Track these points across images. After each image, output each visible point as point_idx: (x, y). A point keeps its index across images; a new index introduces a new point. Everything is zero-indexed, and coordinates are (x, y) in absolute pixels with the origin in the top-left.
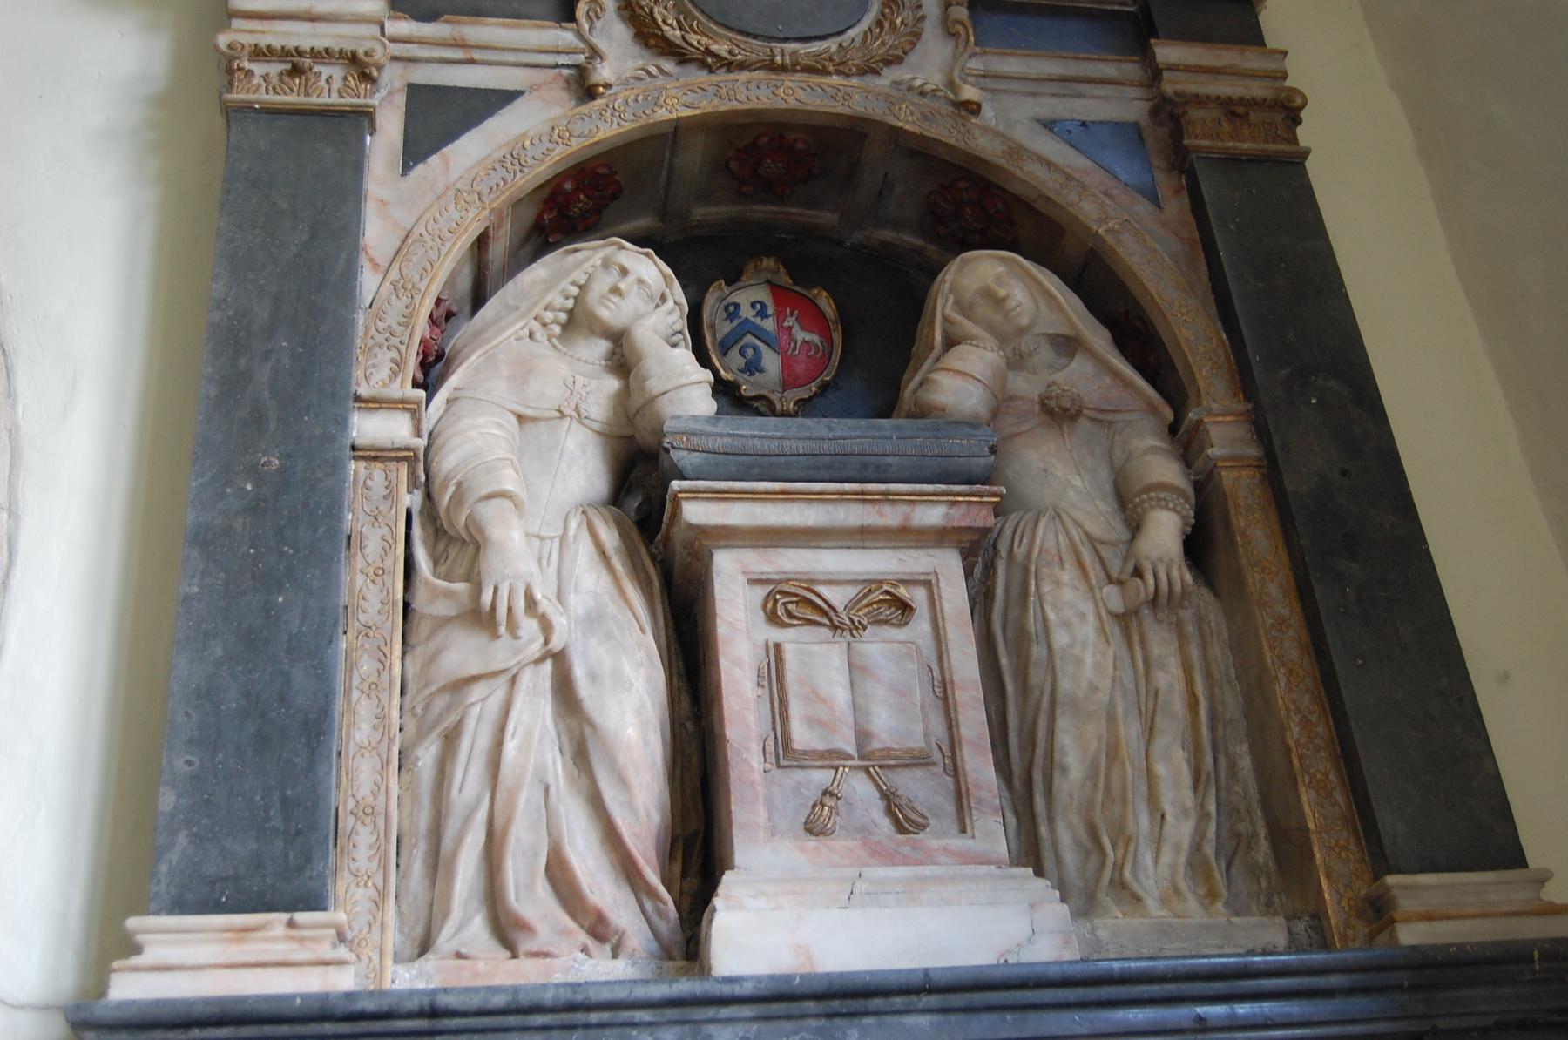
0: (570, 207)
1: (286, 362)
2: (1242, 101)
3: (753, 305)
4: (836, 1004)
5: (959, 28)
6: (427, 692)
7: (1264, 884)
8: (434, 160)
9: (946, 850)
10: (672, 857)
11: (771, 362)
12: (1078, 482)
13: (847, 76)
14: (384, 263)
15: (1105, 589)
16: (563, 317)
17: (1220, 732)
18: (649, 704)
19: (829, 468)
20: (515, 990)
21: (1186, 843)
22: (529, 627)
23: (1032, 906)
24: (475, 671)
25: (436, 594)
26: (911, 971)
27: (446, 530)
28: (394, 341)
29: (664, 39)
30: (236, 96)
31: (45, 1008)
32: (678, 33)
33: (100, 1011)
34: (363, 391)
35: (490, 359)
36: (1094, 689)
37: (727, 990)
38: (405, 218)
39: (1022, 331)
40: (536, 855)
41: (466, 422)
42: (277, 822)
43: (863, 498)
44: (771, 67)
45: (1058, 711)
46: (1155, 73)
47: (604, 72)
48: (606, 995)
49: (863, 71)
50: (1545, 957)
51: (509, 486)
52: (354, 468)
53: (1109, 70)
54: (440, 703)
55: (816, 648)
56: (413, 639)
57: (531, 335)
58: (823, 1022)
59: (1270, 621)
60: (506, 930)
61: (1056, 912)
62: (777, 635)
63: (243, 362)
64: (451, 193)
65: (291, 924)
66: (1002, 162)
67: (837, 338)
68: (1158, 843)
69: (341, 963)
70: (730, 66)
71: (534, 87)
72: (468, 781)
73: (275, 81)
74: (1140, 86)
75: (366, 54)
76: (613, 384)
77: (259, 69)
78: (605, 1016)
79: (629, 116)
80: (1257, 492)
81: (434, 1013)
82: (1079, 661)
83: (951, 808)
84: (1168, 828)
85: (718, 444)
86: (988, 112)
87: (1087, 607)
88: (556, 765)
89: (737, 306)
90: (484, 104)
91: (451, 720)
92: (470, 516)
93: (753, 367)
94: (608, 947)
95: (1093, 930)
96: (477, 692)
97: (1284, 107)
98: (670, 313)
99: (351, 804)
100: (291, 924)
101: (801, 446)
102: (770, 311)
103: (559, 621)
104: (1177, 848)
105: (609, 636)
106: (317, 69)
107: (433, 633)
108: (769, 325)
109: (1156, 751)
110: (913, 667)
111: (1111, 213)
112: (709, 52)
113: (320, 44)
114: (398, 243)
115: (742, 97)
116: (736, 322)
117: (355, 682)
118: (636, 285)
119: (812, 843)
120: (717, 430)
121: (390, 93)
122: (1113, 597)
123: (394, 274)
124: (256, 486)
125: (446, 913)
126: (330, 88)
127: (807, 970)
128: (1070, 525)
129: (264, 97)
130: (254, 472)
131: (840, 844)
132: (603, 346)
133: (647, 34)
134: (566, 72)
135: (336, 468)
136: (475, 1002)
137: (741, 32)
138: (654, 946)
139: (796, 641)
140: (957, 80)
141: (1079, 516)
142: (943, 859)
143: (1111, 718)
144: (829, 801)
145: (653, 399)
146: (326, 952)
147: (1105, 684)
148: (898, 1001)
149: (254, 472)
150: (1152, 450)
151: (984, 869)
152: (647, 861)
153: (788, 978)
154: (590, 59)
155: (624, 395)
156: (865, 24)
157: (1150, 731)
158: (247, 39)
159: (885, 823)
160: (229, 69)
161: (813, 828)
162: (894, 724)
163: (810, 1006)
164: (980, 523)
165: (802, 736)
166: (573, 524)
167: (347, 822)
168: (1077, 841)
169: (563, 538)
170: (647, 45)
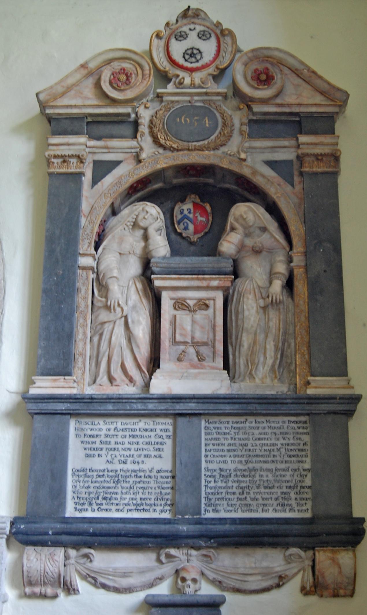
0: (140, 190)
1: (63, 245)
2: (321, 155)
3: (188, 210)
4: (174, 400)
6: (96, 325)
8: (99, 184)
9: (209, 366)
11: (191, 227)
12: (259, 270)
13: (210, 151)
14: (87, 215)
15: (260, 301)
16: (132, 224)
18: (146, 328)
19: (191, 271)
20: (108, 395)
22: (118, 310)
23: (222, 381)
24: (106, 320)
25: (98, 301)
26: (190, 395)
27: (101, 284)
29: (159, 143)
30: (51, 170)
32: (164, 141)
34: (81, 252)
35: (113, 236)
36: (252, 326)
38: (92, 201)
39: (250, 227)
40: (118, 363)
41: (106, 256)
42: (62, 357)
43: (198, 279)
44: (189, 150)
45: (243, 332)
47: (143, 156)
48: (126, 396)
49: (214, 149)
50: (340, 398)
52: (79, 271)
53: (286, 143)
54: (99, 327)
55: (184, 316)
56: (93, 310)
57: (124, 229)
58: (172, 404)
59: (298, 311)
60: (111, 379)
62: (175, 312)
63: (53, 246)
64: (103, 194)
67: (210, 218)
68: (264, 364)
69: (74, 387)
71: (126, 159)
73: (60, 164)
74: (295, 147)
75: (82, 156)
77: (55, 161)
78: (126, 401)
79: (150, 168)
81: (92, 398)
82: (250, 319)
83: (212, 355)
84: (267, 361)
85: (164, 265)
86: (249, 160)
87: (254, 305)
88: (124, 342)
89: (183, 210)
91: (101, 332)
92: (106, 282)
93: (186, 228)
94: (133, 384)
95: (240, 386)
96: (106, 325)
97: (333, 155)
98: (159, 223)
99: (78, 352)
100: (64, 379)
102: (192, 211)
103: (125, 308)
104: (268, 366)
105: (137, 312)
108: (191, 216)
110: (206, 321)
111: (279, 191)
112: (171, 147)
113: (70, 153)
114: (90, 209)
115: (180, 160)
116: (183, 215)
117: (79, 324)
118: (152, 213)
119: (178, 363)
120: (164, 262)
121: (89, 163)
122: (262, 303)
123: (89, 218)
124: (57, 278)
125: (99, 375)
126: (73, 167)
127: (170, 393)
128: (254, 283)
130: (56, 275)
131: (184, 364)
132: (142, 232)
133: (156, 141)
134: (134, 154)
135: (75, 273)
136: (100, 397)
137: (181, 140)
138: (144, 384)
139: (180, 314)
140: (240, 151)
142: (208, 368)
143: (255, 334)
144: (183, 353)
145: (150, 251)
146: (72, 385)
147: (255, 325)
148: (188, 400)
149: (56, 275)
151: (216, 371)
152: (143, 365)
153: (164, 395)
154: (140, 150)
155: (146, 247)
156: (215, 135)
157: (266, 337)
158: (52, 153)
159: (196, 359)
160: (49, 163)
161: (179, 360)
163: (169, 400)
164: (227, 285)
165: (178, 338)
166: (131, 283)
167: (77, 356)
168: (244, 363)
169: (128, 286)
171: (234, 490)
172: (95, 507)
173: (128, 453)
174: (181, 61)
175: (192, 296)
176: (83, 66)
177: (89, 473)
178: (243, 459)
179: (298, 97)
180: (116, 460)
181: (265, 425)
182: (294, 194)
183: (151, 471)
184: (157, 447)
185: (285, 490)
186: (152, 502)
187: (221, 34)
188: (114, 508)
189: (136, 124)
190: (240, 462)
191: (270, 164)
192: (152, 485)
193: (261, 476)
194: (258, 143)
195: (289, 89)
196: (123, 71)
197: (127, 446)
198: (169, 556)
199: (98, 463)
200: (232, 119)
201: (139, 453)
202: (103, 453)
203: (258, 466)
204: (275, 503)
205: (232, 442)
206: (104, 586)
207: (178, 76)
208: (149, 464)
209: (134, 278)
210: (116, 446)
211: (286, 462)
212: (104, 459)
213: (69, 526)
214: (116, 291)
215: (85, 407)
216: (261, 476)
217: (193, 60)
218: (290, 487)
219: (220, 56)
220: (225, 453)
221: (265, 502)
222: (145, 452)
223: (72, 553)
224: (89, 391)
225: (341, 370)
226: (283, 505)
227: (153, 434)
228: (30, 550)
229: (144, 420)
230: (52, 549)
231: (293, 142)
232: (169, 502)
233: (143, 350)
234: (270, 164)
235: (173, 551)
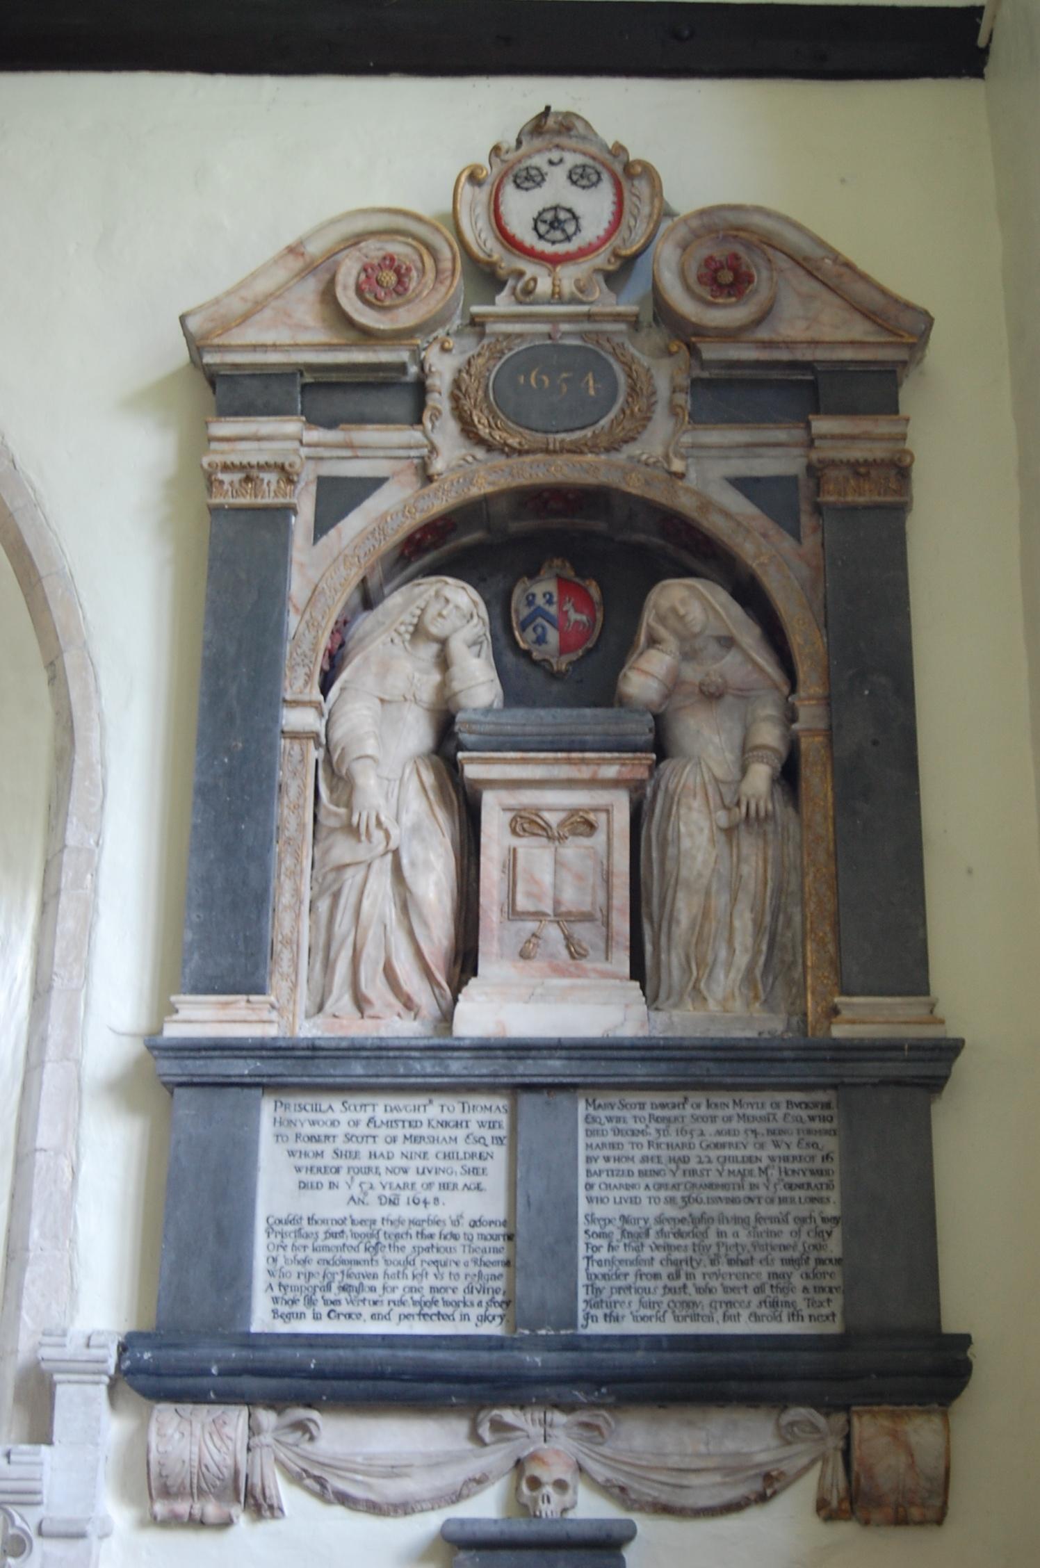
0: (433, 547)
2: (866, 463)
3: (544, 595)
4: (513, 1053)
5: (679, 410)
7: (794, 991)
8: (332, 532)
9: (595, 970)
10: (455, 962)
11: (553, 636)
12: (716, 739)
14: (301, 607)
16: (411, 629)
17: (783, 899)
19: (552, 742)
21: (743, 967)
22: (378, 835)
23: (627, 1006)
24: (348, 861)
25: (330, 813)
27: (336, 773)
28: (307, 661)
29: (477, 434)
31: (134, 1035)
33: (160, 1041)
34: (288, 697)
35: (366, 659)
36: (700, 875)
37: (456, 1043)
38: (314, 574)
39: (695, 636)
40: (378, 963)
42: (242, 948)
43: (569, 761)
44: (547, 451)
48: (396, 1043)
49: (607, 450)
50: (911, 1048)
51: (370, 752)
52: (284, 743)
53: (781, 435)
54: (331, 877)
55: (536, 851)
56: (318, 836)
57: (392, 641)
58: (506, 1061)
60: (360, 1002)
61: (640, 1008)
62: (515, 842)
63: (221, 682)
64: (341, 558)
65: (248, 1001)
67: (599, 615)
68: (729, 965)
69: (271, 1022)
70: (521, 452)
71: (395, 474)
72: (343, 922)
73: (237, 485)
75: (291, 465)
76: (436, 677)
77: (226, 477)
78: (397, 1053)
79: (453, 494)
80: (823, 752)
82: (694, 858)
83: (602, 945)
85: (488, 728)
86: (692, 475)
87: (705, 824)
89: (534, 595)
91: (335, 888)
92: (348, 770)
93: (541, 640)
94: (412, 1014)
96: (349, 872)
98: (476, 626)
100: (248, 1001)
101: (534, 729)
102: (555, 599)
103: (394, 832)
105: (423, 840)
106: (262, 475)
107: (326, 838)
108: (553, 610)
109: (736, 914)
110: (590, 863)
112: (506, 444)
113: (262, 459)
116: (532, 608)
117: (283, 870)
118: (457, 605)
119: (521, 963)
121: (307, 484)
122: (722, 818)
123: (307, 616)
124: (230, 760)
125: (330, 992)
126: (270, 492)
128: (704, 769)
129: (231, 500)
131: (537, 964)
132: (434, 648)
133: (468, 431)
135: (272, 747)
136: (333, 1044)
137: (528, 428)
138: (438, 1013)
140: (671, 455)
141: (712, 764)
143: (708, 894)
144: (534, 940)
146: (265, 1015)
148: (545, 1053)
150: (767, 718)
153: (488, 1039)
155: (444, 685)
156: (611, 415)
157: (734, 900)
158: (219, 459)
159: (565, 953)
160: (211, 483)
161: (524, 955)
162: (571, 898)
163: (499, 1053)
164: (639, 776)
165: (522, 903)
166: (407, 771)
167: (278, 947)
170: (468, 437)
172: (322, 1309)
173: (400, 1179)
174: (529, 239)
177: (307, 1228)
178: (678, 1194)
179: (810, 325)
180: (372, 1197)
183: (456, 1223)
184: (471, 1164)
185: (778, 1268)
186: (459, 1296)
188: (367, 1310)
189: (420, 389)
191: (744, 485)
192: (460, 1255)
193: (720, 1234)
194: (713, 436)
195: (790, 306)
196: (390, 262)
197: (398, 1162)
198: (499, 1427)
199: (330, 1204)
201: (427, 1178)
202: (342, 1178)
203: (713, 1210)
204: (756, 1299)
205: (653, 1152)
206: (343, 1499)
207: (520, 274)
209: (416, 758)
210: (373, 1163)
211: (782, 1200)
212: (343, 1193)
214: (373, 791)
215: (300, 1069)
216: (720, 1234)
217: (558, 235)
218: (791, 1261)
219: (623, 227)
220: (635, 1179)
222: (443, 1178)
223: (267, 1418)
225: (907, 970)
226: (774, 1304)
227: (461, 1133)
228: (165, 1413)
229: (439, 1100)
230: (218, 1410)
231: (798, 434)
232: (499, 1298)
234: (744, 485)
235: (509, 1416)
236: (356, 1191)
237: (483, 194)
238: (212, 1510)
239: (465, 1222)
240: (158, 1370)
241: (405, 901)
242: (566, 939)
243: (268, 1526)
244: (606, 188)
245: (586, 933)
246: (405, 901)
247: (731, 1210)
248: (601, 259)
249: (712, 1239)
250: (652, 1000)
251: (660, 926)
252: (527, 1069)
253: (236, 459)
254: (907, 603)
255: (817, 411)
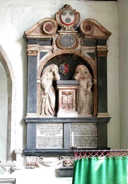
0: (51, 61)
8: (42, 59)
27: (43, 89)
46: (96, 49)
47: (54, 51)
60: (45, 114)
62: (63, 96)
66: (83, 57)
76: (53, 76)
77: (34, 52)
87: (83, 94)
90: (45, 53)
93: (63, 71)
96: (44, 99)
108: (64, 68)
118: (55, 68)
132: (52, 73)
165: (64, 102)
171: (78, 141)
172: (43, 146)
173: (51, 132)
174: (65, 22)
175: (67, 91)
176: (38, 23)
177: (42, 138)
178: (80, 134)
179: (97, 33)
180: (48, 135)
181: (86, 125)
182: (95, 62)
183: (57, 137)
184: (59, 131)
185: (91, 141)
186: (58, 145)
187: (76, 14)
188: (48, 146)
189: (52, 41)
190: (80, 134)
191: (88, 53)
192: (58, 141)
193: (85, 138)
194: (86, 48)
195: (95, 32)
196: (49, 25)
197: (51, 131)
198: (62, 158)
199: (44, 135)
200: (78, 40)
201: (54, 132)
202: (45, 133)
203: (84, 135)
204: (88, 144)
205: (78, 129)
206: (46, 165)
207: (64, 27)
208: (57, 135)
209: (51, 86)
210: (48, 131)
211: (91, 134)
212: (45, 134)
213: (38, 151)
214: (47, 91)
215: (39, 121)
216: (85, 138)
217: (68, 22)
218: (92, 141)
219: (76, 21)
220: (76, 132)
221: (86, 144)
222: (56, 132)
223: (38, 157)
224: (41, 117)
225: (105, 110)
226: (90, 145)
227: (58, 128)
228: (28, 157)
229: (55, 124)
230: (33, 157)
231: (95, 47)
232: (62, 145)
233: (53, 106)
234: (88, 53)
235: (63, 157)
236: (47, 134)
237: (59, 16)
238: (33, 167)
239: (58, 137)
240: (26, 153)
241: (50, 102)
242: (69, 107)
243: (38, 168)
244: (74, 16)
245: (70, 106)
246: (50, 102)
247: (86, 135)
248: (73, 25)
249: (84, 138)
250: (79, 113)
251: (77, 105)
252: (65, 121)
253: (31, 50)
254: (107, 68)
255: (97, 45)
